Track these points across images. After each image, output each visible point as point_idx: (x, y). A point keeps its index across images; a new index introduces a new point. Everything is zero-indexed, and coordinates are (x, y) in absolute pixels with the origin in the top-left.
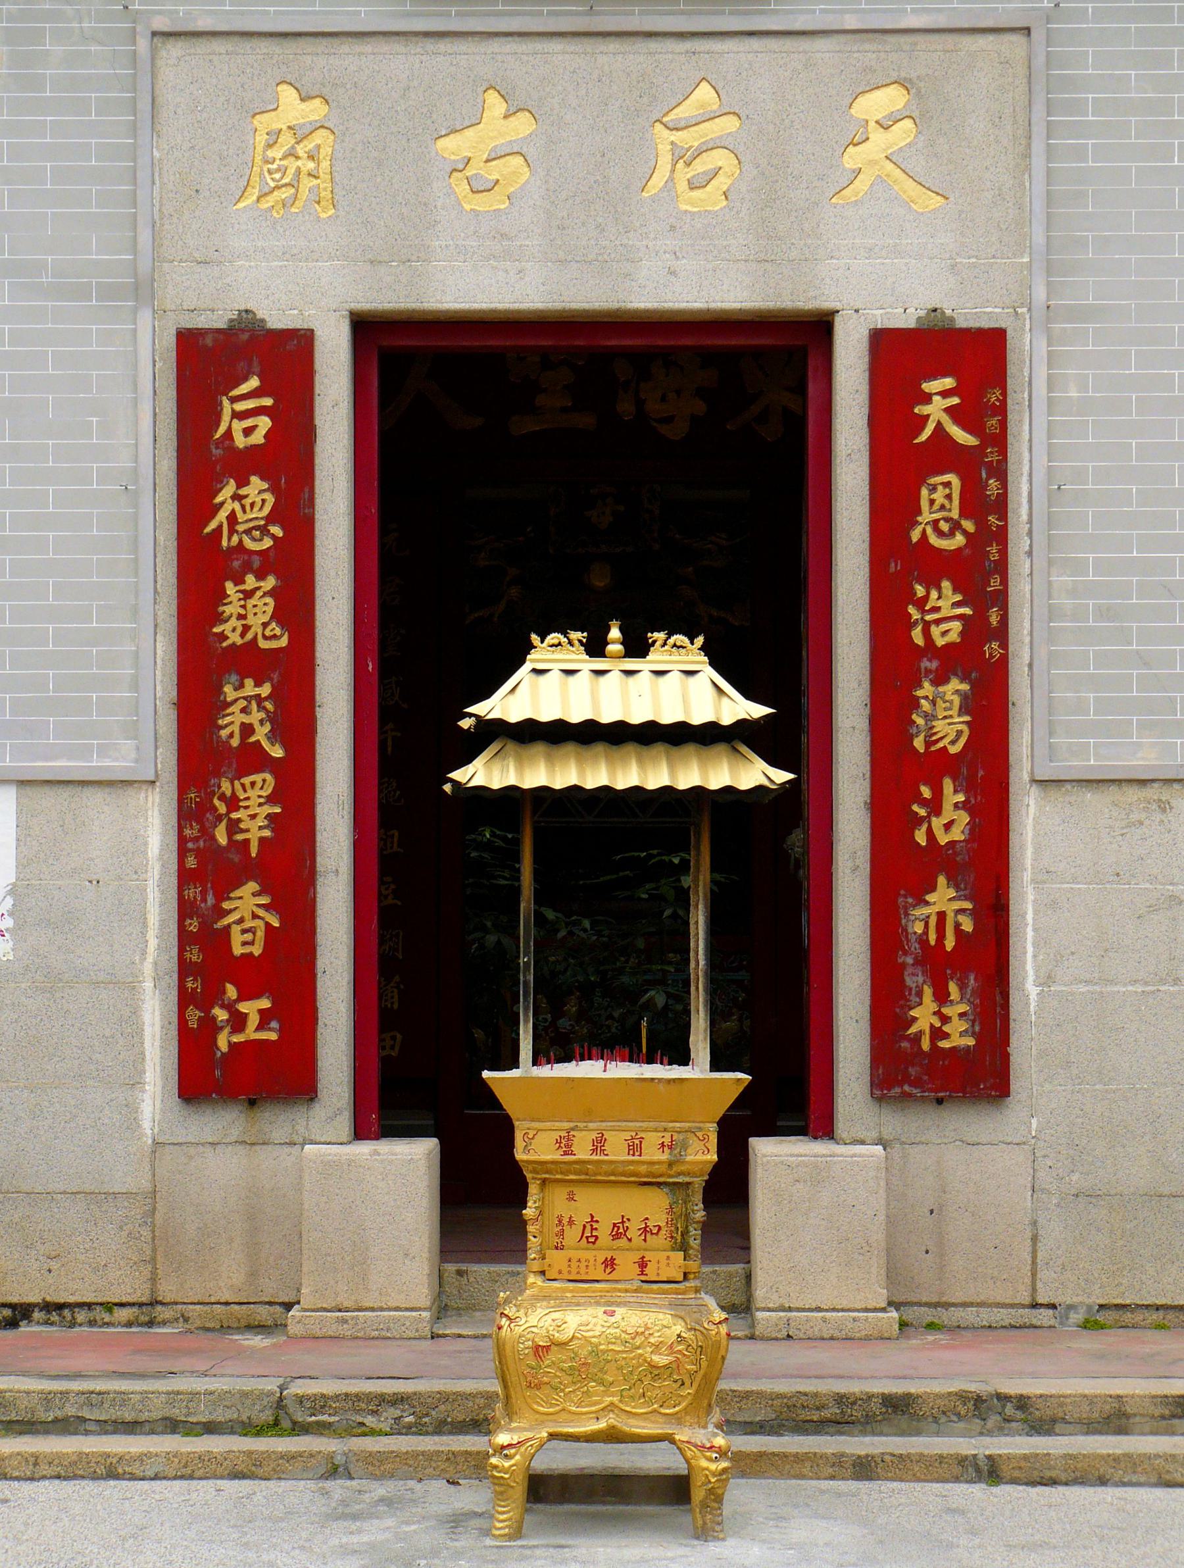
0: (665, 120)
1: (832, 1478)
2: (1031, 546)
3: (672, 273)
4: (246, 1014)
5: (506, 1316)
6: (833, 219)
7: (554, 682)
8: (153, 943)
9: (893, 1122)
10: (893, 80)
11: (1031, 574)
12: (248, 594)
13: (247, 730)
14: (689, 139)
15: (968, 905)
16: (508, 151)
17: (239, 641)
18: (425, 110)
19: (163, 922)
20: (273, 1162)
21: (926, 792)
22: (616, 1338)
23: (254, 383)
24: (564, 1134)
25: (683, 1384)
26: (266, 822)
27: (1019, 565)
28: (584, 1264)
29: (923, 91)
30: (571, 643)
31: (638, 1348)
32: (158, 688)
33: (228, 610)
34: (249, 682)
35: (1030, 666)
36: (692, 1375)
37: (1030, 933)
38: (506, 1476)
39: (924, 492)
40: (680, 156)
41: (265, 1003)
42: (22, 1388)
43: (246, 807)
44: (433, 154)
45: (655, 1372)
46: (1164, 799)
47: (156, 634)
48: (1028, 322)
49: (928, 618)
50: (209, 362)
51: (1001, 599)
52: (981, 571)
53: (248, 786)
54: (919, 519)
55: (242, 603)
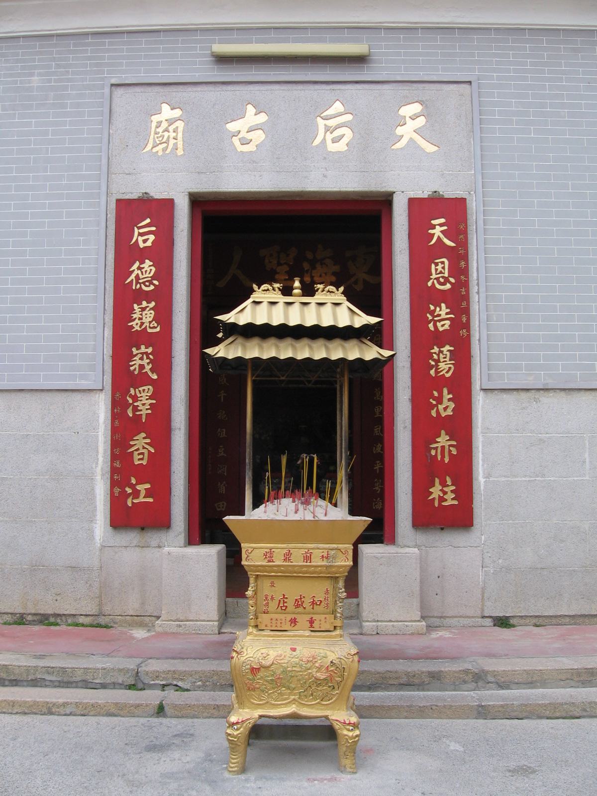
0: (322, 115)
1: (406, 718)
2: (478, 289)
3: (325, 176)
4: (140, 490)
5: (236, 651)
6: (392, 155)
7: (264, 306)
8: (101, 459)
9: (422, 537)
10: (415, 101)
11: (479, 302)
12: (143, 309)
13: (142, 367)
14: (332, 123)
15: (454, 443)
16: (256, 128)
17: (139, 329)
18: (222, 112)
19: (105, 451)
20: (151, 554)
21: (436, 394)
22: (296, 664)
23: (148, 221)
24: (268, 550)
25: (334, 688)
26: (149, 407)
27: (474, 298)
28: (279, 622)
29: (428, 105)
30: (274, 289)
31: (309, 669)
32: (105, 350)
33: (134, 316)
34: (143, 347)
35: (479, 340)
36: (339, 683)
37: (480, 455)
38: (235, 740)
39: (433, 266)
40: (327, 129)
41: (148, 486)
42: (16, 664)
43: (141, 400)
44: (225, 130)
45: (318, 682)
46: (536, 397)
47: (104, 327)
48: (474, 197)
49: (435, 319)
50: (130, 211)
51: (467, 311)
52: (459, 299)
53: (142, 391)
54: (431, 277)
55: (141, 313)
